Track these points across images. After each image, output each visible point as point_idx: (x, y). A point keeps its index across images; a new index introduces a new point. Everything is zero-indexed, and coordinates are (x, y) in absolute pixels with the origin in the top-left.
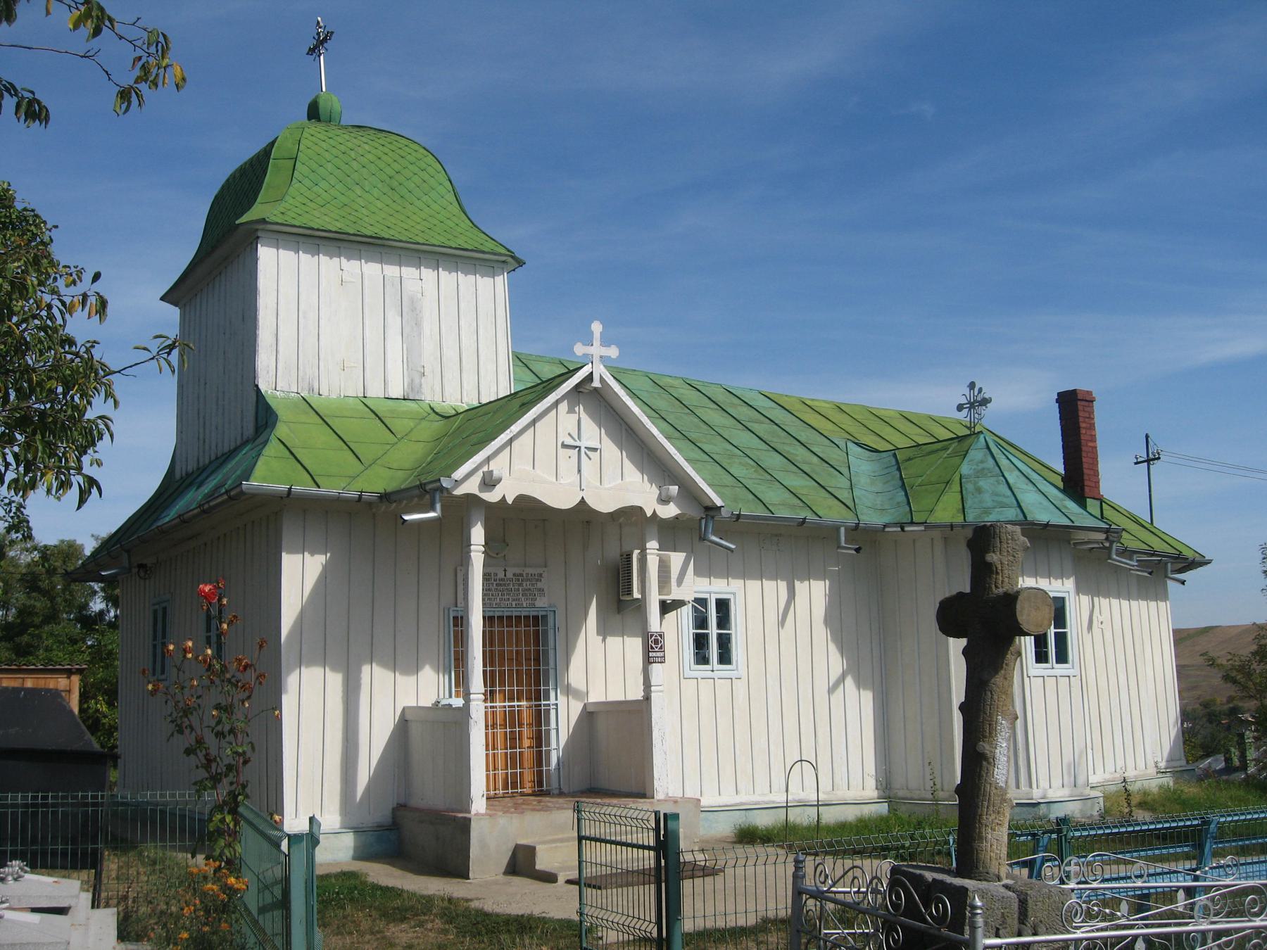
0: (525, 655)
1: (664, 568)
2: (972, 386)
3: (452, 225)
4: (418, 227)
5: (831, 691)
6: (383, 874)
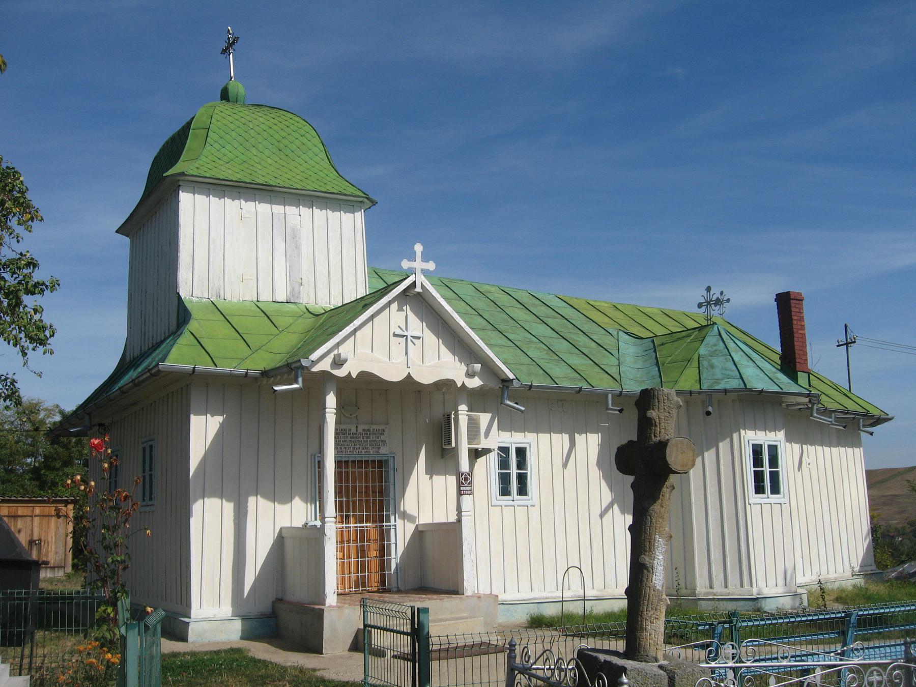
0: (369, 489)
1: (473, 427)
2: (709, 289)
3: (323, 175)
4: (298, 177)
5: (602, 516)
6: (261, 651)
